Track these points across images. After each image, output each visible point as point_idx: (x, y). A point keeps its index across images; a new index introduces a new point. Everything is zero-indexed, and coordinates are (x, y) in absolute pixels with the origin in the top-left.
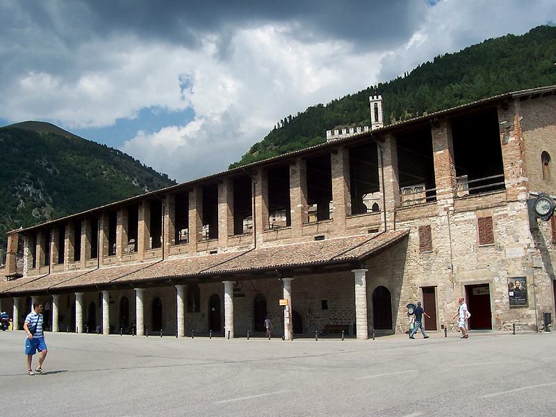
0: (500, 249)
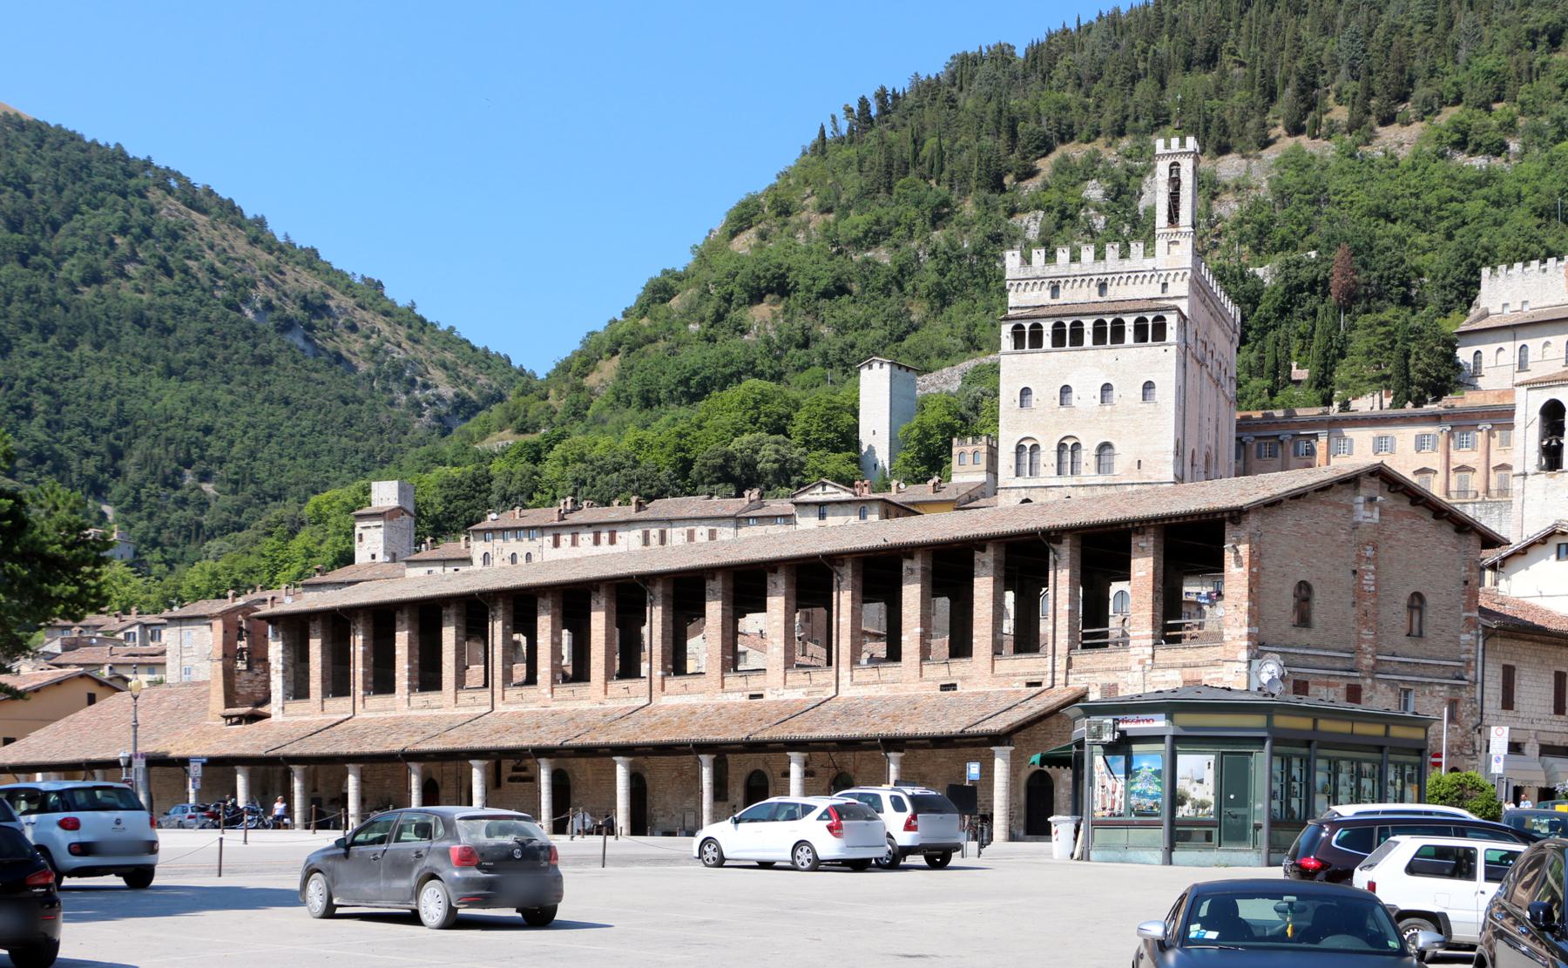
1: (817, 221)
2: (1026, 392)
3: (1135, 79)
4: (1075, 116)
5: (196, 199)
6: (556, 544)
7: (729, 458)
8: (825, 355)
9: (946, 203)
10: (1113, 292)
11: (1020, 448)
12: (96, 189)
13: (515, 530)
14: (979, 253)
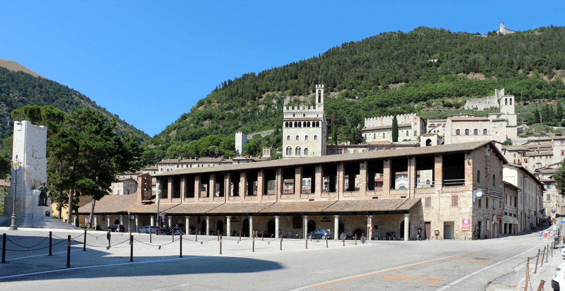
0: (460, 208)
1: (217, 105)
2: (289, 137)
3: (281, 80)
4: (270, 87)
5: (82, 97)
6: (178, 167)
7: (208, 151)
8: (221, 131)
9: (244, 102)
10: (307, 116)
11: (287, 149)
12: (62, 94)
13: (168, 164)
14: (253, 112)
